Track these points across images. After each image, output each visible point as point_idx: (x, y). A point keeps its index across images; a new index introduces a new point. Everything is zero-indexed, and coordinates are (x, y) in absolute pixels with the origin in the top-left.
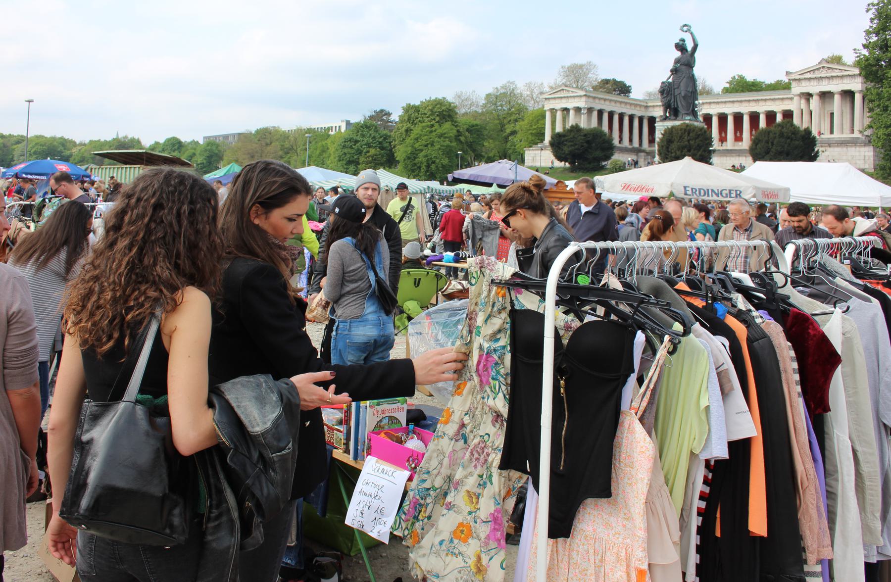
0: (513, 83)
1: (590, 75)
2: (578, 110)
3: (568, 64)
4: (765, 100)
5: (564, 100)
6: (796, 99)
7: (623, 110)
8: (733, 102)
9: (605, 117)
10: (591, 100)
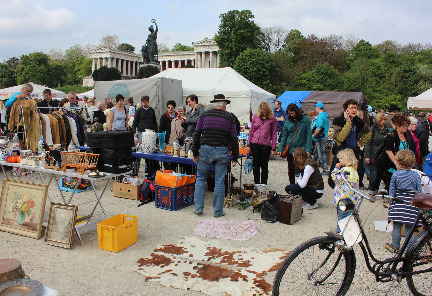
0: (79, 45)
1: (115, 42)
2: (106, 58)
3: (105, 36)
4: (187, 55)
5: (101, 54)
6: (196, 54)
7: (128, 59)
8: (174, 55)
9: (120, 62)
10: (113, 54)
